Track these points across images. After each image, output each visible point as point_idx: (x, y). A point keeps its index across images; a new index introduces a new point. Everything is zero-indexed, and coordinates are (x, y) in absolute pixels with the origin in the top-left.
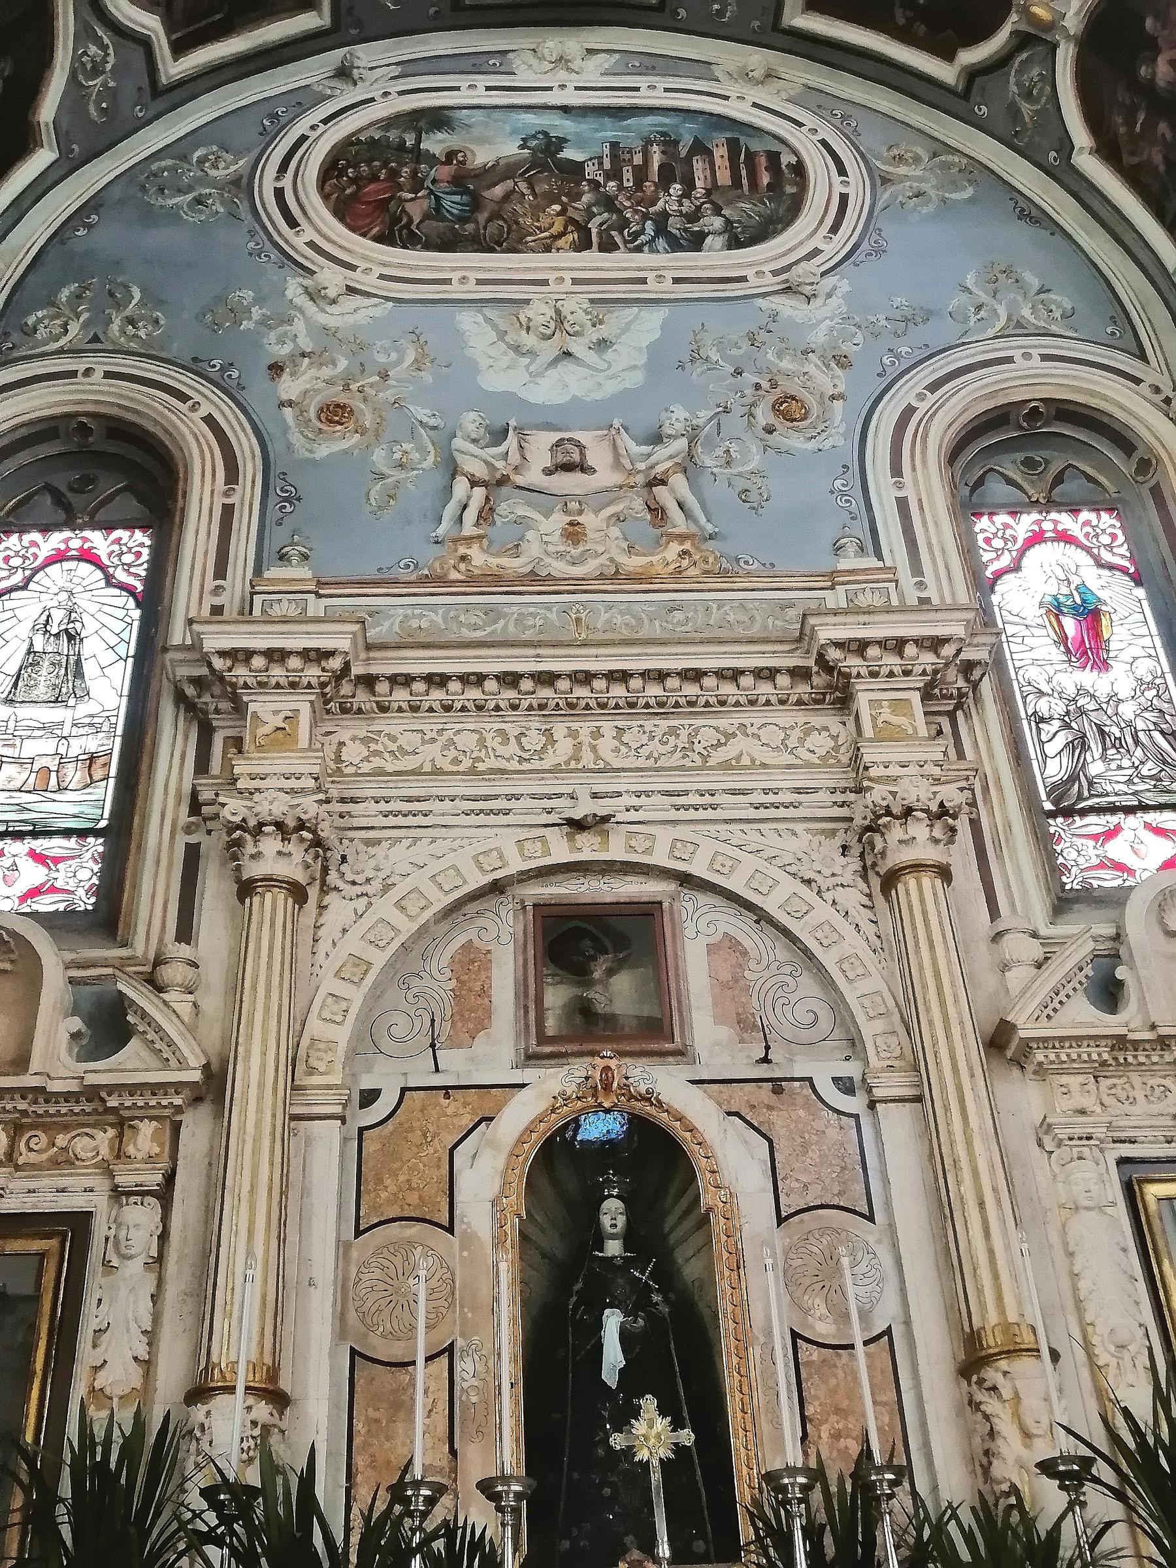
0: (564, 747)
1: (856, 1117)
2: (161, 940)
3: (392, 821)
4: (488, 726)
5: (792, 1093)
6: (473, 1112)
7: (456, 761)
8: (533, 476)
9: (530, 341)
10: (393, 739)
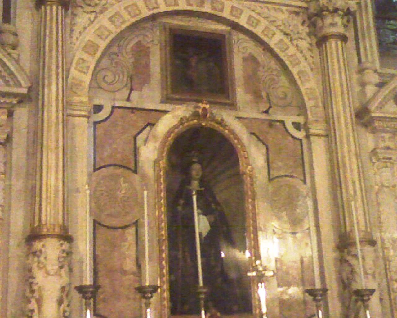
1: (300, 140)
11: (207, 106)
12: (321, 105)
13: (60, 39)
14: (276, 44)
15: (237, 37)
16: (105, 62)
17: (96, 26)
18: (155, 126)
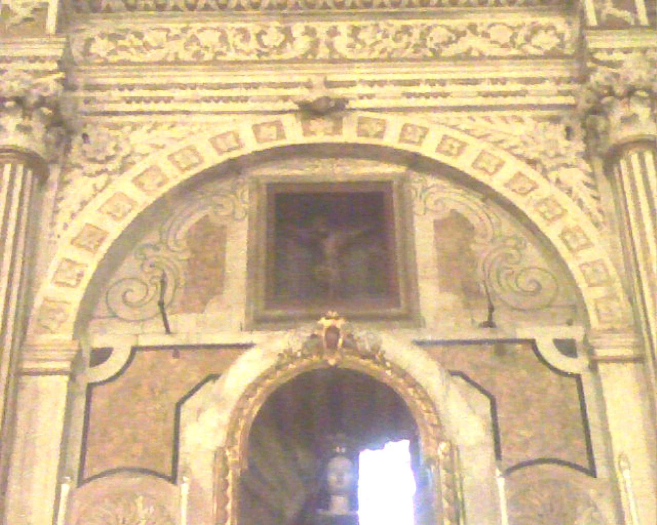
0: (301, 44)
1: (578, 377)
3: (135, 107)
4: (230, 25)
5: (514, 354)
6: (202, 370)
7: (197, 55)
10: (139, 35)
11: (340, 323)
12: (621, 295)
14: (506, 185)
15: (419, 182)
18: (221, 379)
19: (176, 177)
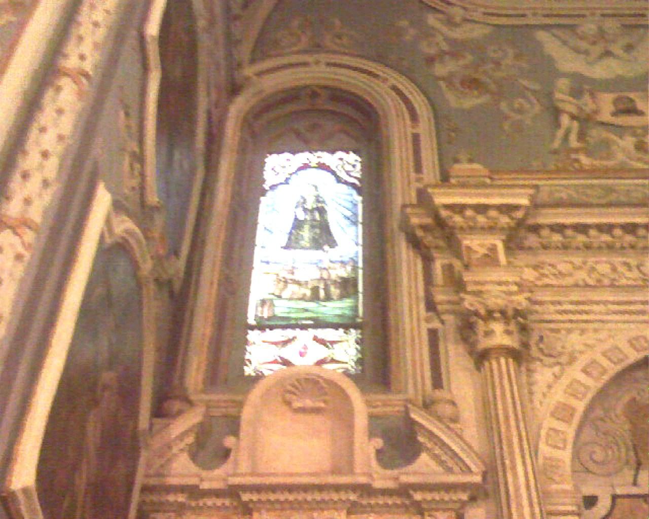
2: (424, 391)
8: (606, 115)
9: (584, 45)
13: (518, 402)
16: (588, 434)
17: (565, 381)
19: (613, 369)
